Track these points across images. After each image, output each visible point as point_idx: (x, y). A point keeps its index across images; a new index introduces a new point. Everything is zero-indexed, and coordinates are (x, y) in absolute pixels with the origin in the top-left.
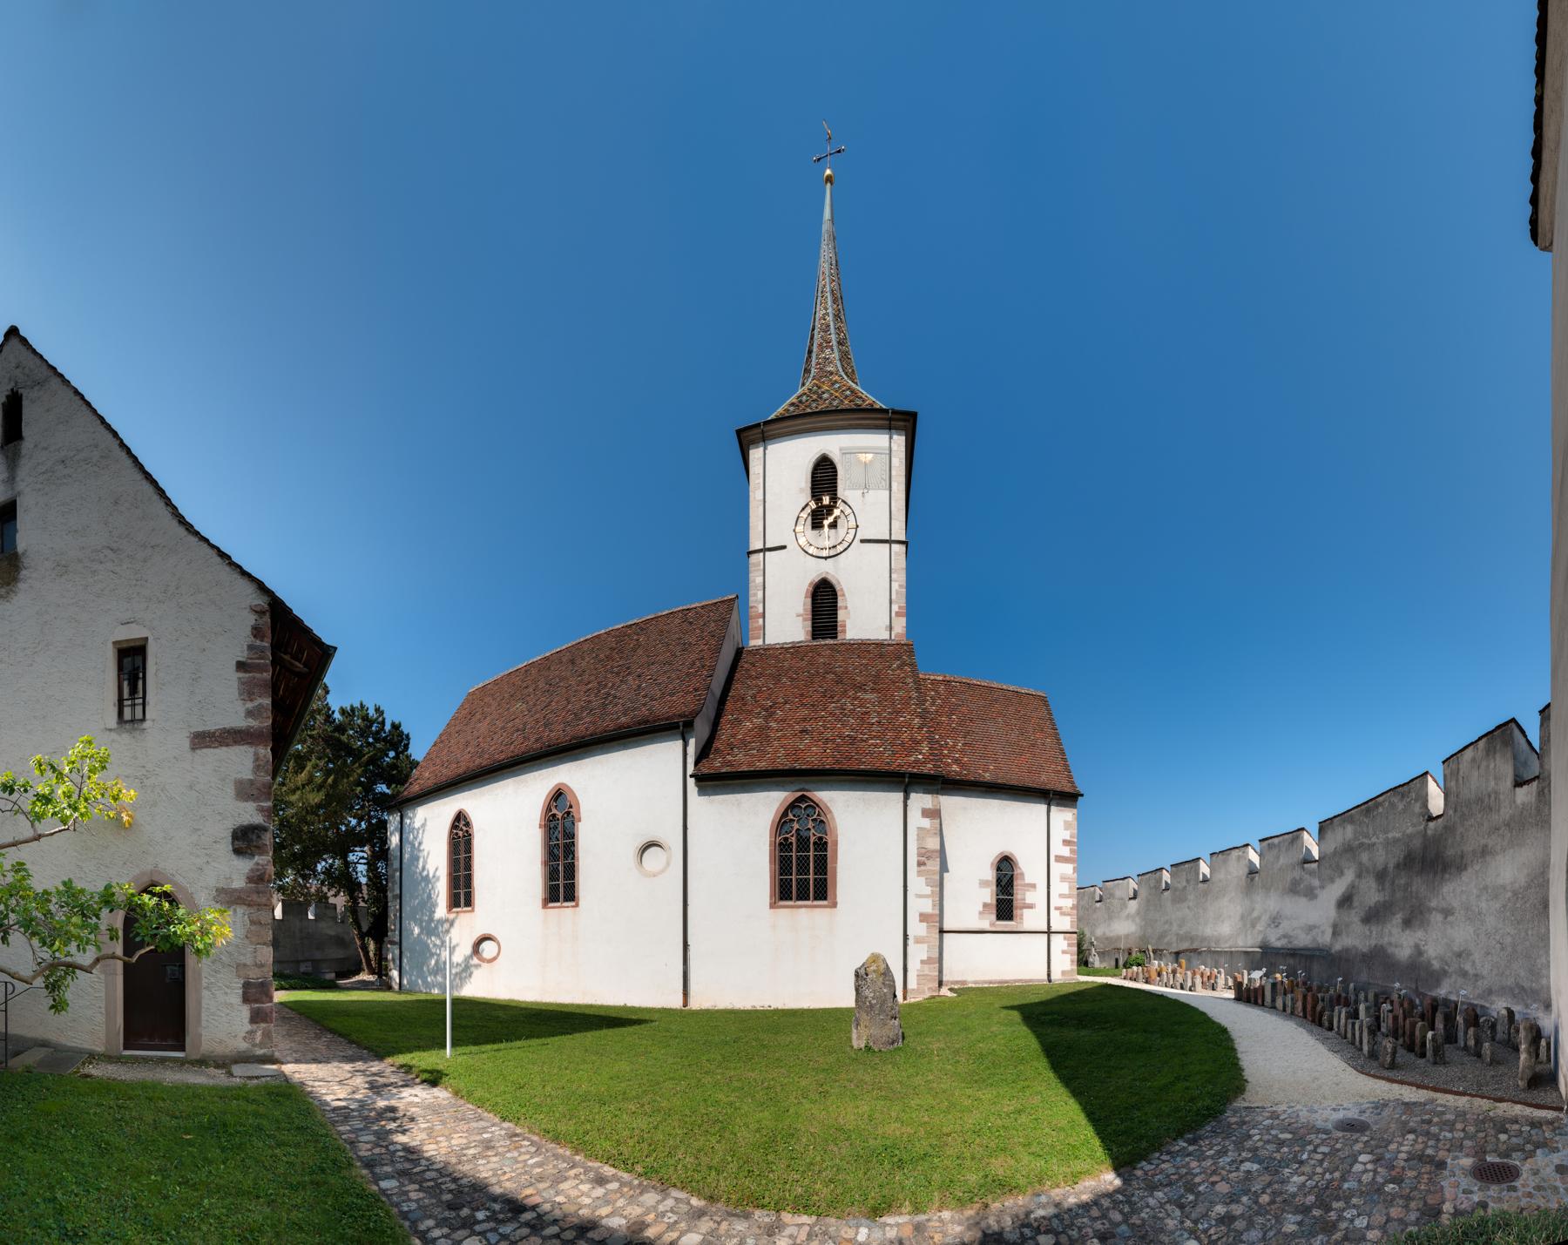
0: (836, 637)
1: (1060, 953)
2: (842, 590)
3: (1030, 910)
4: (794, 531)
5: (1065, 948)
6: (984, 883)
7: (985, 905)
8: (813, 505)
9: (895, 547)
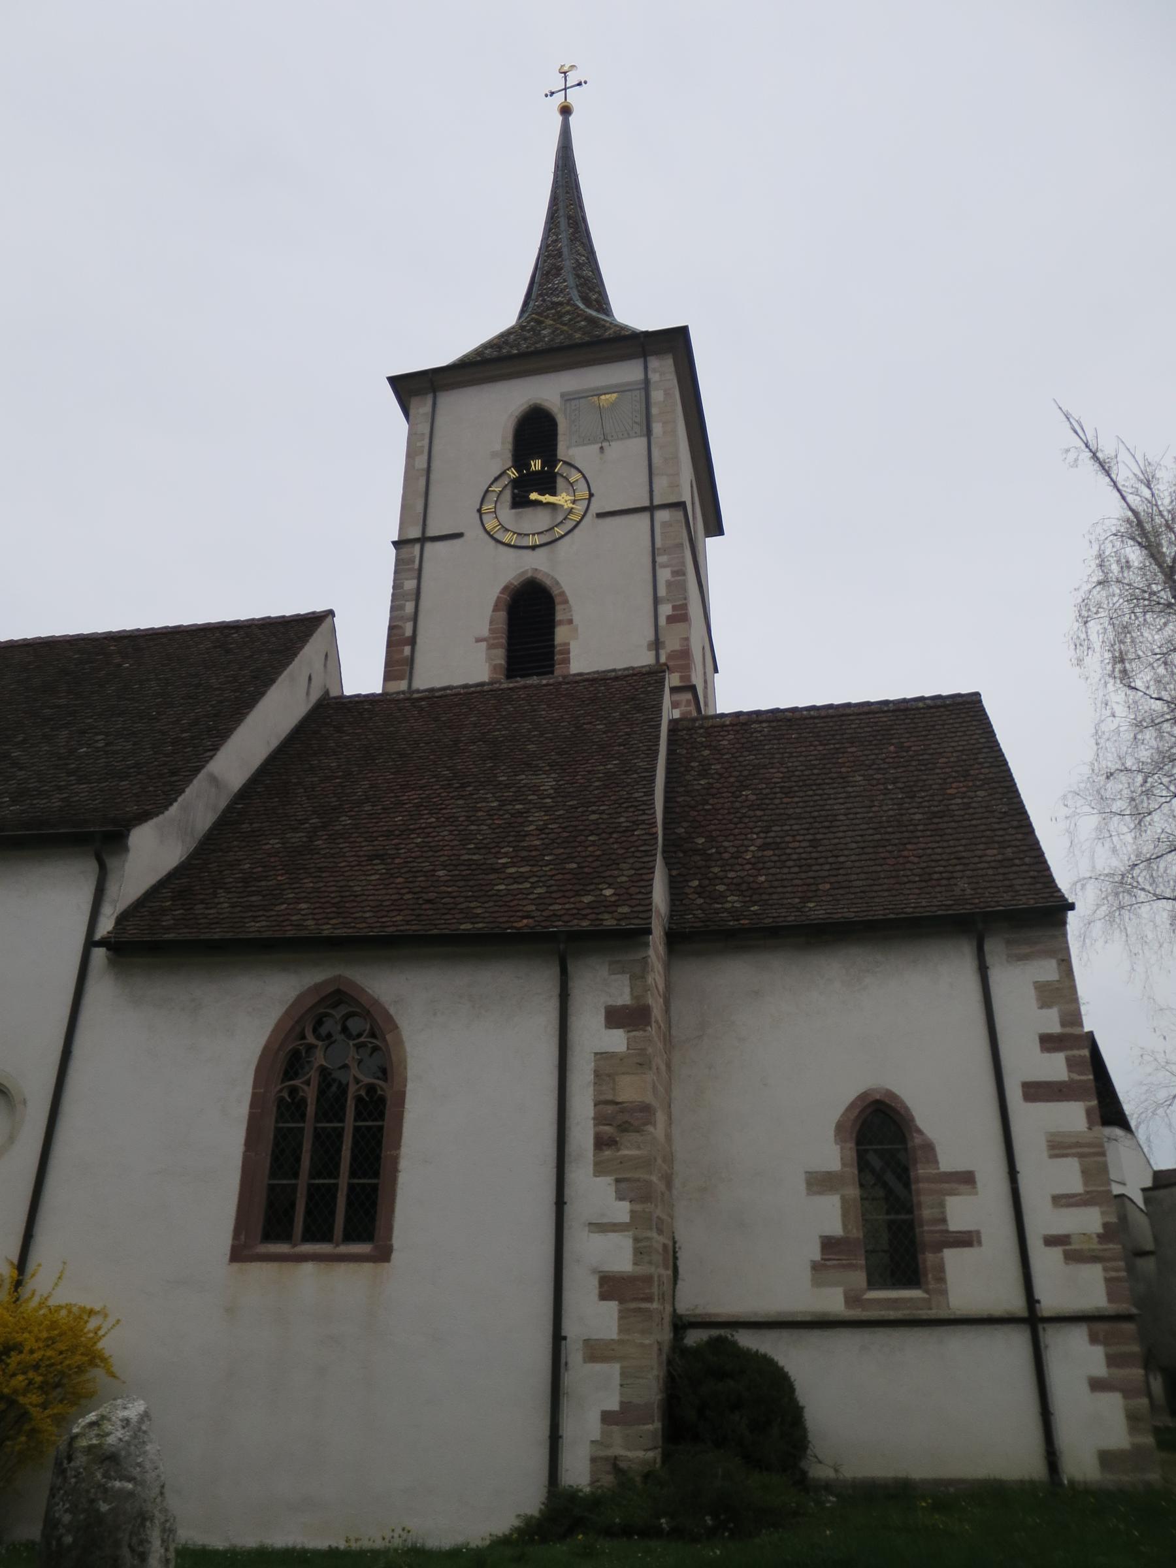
0: (552, 672)
1: (1085, 1387)
2: (563, 594)
3: (966, 1251)
4: (479, 511)
5: (1100, 1369)
6: (819, 1183)
7: (829, 1244)
8: (513, 474)
9: (662, 516)
